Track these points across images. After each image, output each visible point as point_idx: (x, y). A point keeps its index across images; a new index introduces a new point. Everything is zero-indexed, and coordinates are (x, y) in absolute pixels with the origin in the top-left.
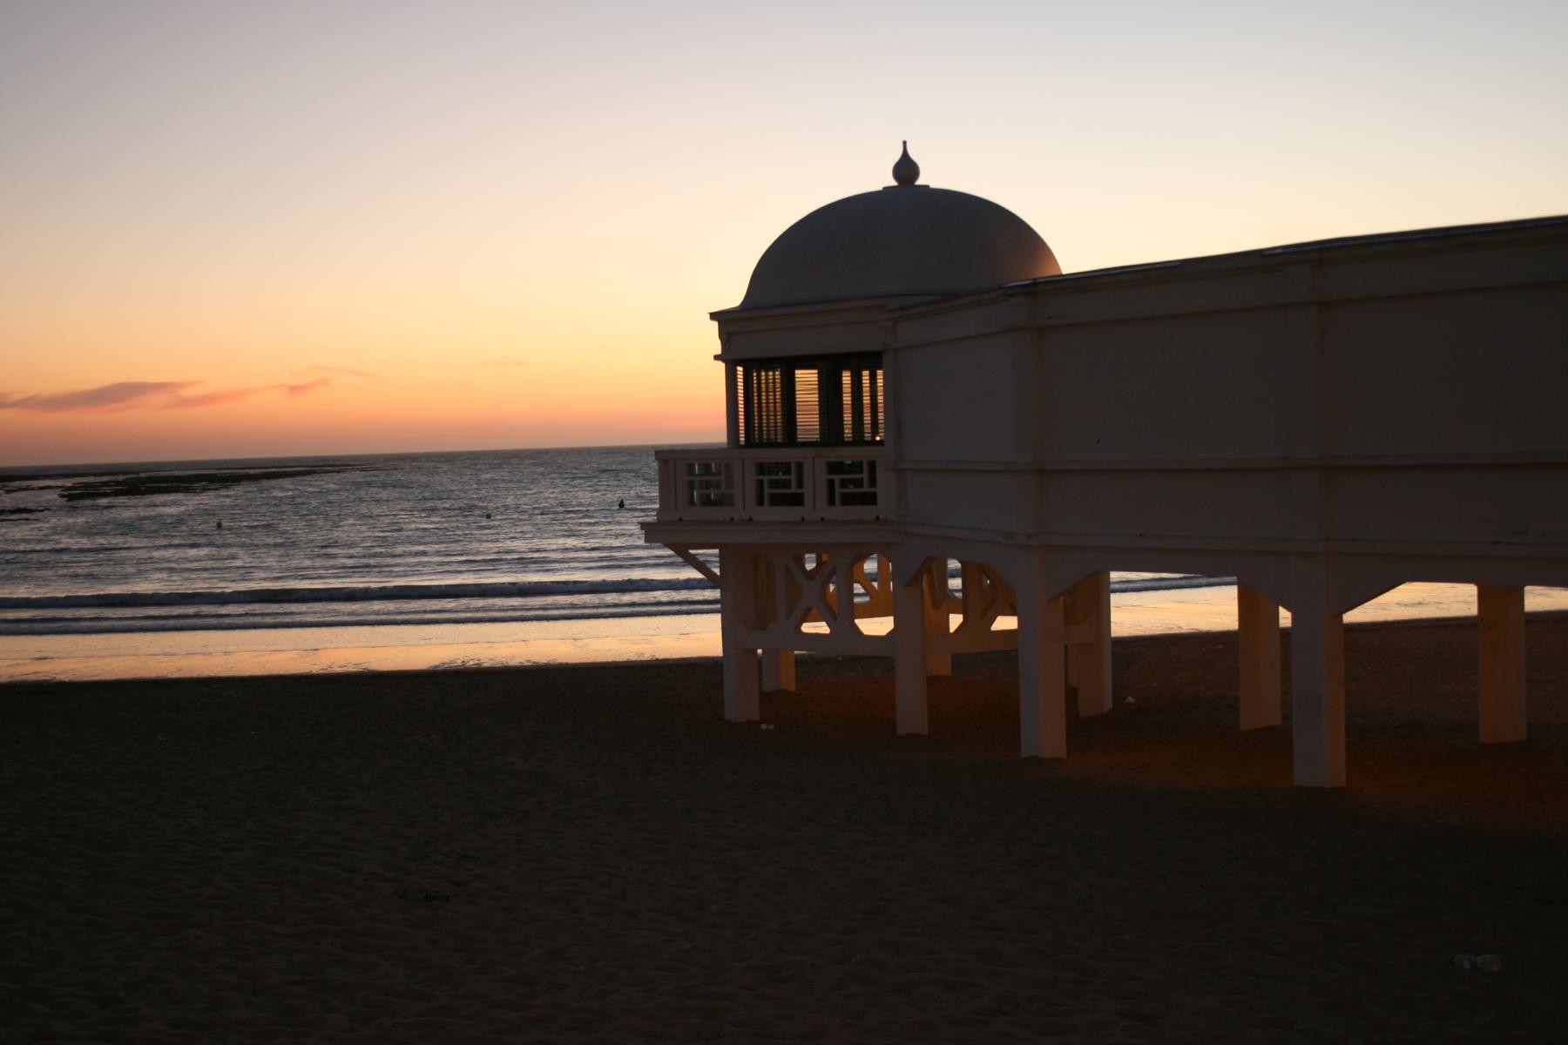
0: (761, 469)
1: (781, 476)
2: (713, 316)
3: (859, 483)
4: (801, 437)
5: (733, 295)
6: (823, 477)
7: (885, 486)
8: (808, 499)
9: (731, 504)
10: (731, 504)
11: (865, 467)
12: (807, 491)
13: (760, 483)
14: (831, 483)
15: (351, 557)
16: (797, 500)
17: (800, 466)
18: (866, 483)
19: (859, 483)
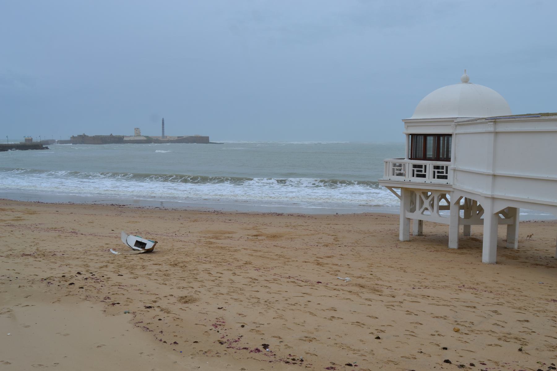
0: (415, 166)
1: (440, 170)
2: (263, 345)
3: (421, 171)
4: (428, 156)
5: (114, 135)
6: (411, 168)
7: (450, 174)
8: (427, 176)
9: (405, 176)
10: (405, 176)
11: (423, 167)
12: (427, 174)
13: (414, 170)
14: (434, 172)
15: (140, 186)
16: (424, 176)
17: (425, 166)
18: (423, 171)
19: (438, 172)
